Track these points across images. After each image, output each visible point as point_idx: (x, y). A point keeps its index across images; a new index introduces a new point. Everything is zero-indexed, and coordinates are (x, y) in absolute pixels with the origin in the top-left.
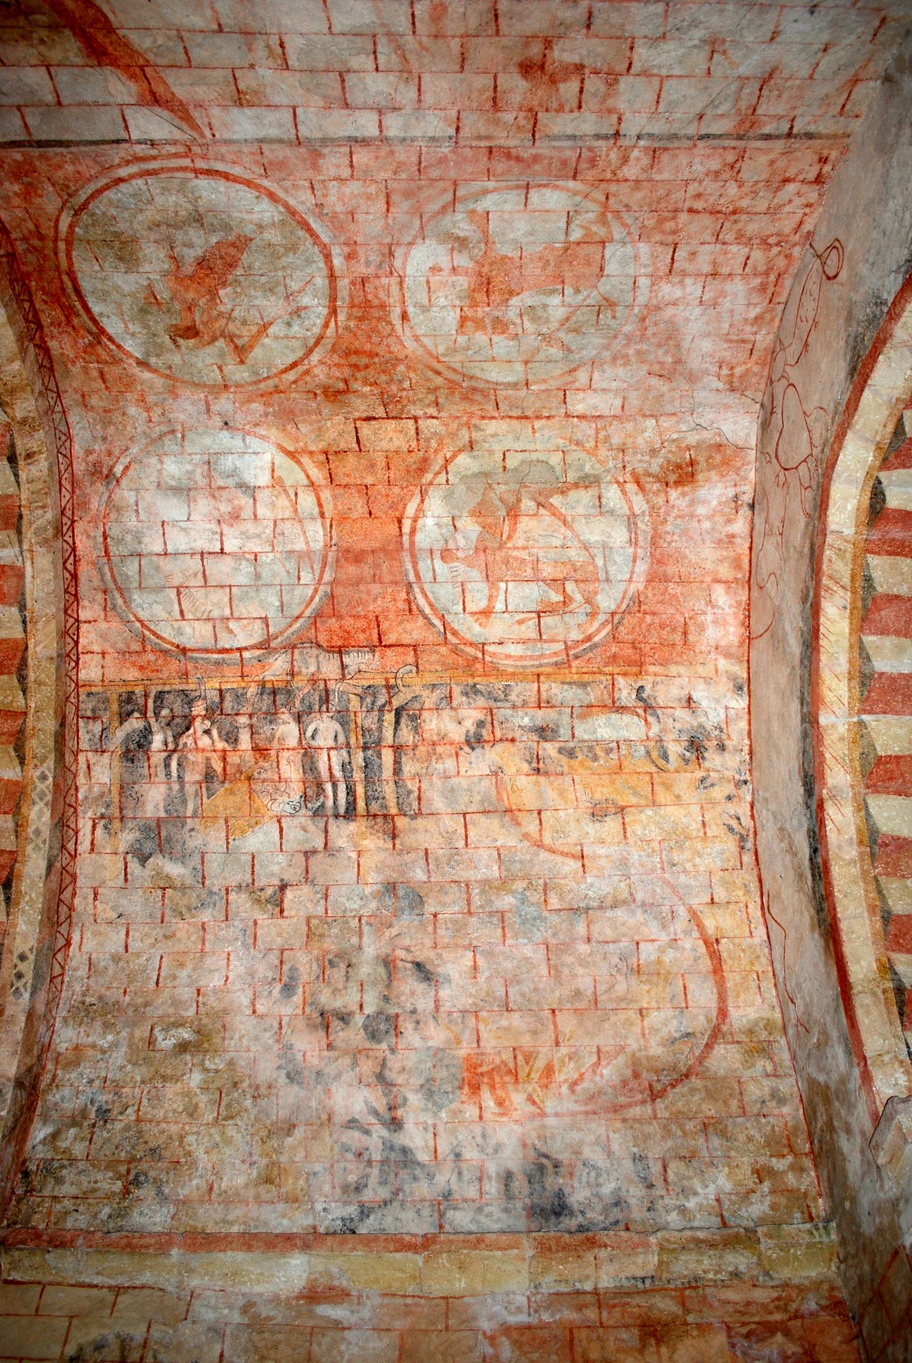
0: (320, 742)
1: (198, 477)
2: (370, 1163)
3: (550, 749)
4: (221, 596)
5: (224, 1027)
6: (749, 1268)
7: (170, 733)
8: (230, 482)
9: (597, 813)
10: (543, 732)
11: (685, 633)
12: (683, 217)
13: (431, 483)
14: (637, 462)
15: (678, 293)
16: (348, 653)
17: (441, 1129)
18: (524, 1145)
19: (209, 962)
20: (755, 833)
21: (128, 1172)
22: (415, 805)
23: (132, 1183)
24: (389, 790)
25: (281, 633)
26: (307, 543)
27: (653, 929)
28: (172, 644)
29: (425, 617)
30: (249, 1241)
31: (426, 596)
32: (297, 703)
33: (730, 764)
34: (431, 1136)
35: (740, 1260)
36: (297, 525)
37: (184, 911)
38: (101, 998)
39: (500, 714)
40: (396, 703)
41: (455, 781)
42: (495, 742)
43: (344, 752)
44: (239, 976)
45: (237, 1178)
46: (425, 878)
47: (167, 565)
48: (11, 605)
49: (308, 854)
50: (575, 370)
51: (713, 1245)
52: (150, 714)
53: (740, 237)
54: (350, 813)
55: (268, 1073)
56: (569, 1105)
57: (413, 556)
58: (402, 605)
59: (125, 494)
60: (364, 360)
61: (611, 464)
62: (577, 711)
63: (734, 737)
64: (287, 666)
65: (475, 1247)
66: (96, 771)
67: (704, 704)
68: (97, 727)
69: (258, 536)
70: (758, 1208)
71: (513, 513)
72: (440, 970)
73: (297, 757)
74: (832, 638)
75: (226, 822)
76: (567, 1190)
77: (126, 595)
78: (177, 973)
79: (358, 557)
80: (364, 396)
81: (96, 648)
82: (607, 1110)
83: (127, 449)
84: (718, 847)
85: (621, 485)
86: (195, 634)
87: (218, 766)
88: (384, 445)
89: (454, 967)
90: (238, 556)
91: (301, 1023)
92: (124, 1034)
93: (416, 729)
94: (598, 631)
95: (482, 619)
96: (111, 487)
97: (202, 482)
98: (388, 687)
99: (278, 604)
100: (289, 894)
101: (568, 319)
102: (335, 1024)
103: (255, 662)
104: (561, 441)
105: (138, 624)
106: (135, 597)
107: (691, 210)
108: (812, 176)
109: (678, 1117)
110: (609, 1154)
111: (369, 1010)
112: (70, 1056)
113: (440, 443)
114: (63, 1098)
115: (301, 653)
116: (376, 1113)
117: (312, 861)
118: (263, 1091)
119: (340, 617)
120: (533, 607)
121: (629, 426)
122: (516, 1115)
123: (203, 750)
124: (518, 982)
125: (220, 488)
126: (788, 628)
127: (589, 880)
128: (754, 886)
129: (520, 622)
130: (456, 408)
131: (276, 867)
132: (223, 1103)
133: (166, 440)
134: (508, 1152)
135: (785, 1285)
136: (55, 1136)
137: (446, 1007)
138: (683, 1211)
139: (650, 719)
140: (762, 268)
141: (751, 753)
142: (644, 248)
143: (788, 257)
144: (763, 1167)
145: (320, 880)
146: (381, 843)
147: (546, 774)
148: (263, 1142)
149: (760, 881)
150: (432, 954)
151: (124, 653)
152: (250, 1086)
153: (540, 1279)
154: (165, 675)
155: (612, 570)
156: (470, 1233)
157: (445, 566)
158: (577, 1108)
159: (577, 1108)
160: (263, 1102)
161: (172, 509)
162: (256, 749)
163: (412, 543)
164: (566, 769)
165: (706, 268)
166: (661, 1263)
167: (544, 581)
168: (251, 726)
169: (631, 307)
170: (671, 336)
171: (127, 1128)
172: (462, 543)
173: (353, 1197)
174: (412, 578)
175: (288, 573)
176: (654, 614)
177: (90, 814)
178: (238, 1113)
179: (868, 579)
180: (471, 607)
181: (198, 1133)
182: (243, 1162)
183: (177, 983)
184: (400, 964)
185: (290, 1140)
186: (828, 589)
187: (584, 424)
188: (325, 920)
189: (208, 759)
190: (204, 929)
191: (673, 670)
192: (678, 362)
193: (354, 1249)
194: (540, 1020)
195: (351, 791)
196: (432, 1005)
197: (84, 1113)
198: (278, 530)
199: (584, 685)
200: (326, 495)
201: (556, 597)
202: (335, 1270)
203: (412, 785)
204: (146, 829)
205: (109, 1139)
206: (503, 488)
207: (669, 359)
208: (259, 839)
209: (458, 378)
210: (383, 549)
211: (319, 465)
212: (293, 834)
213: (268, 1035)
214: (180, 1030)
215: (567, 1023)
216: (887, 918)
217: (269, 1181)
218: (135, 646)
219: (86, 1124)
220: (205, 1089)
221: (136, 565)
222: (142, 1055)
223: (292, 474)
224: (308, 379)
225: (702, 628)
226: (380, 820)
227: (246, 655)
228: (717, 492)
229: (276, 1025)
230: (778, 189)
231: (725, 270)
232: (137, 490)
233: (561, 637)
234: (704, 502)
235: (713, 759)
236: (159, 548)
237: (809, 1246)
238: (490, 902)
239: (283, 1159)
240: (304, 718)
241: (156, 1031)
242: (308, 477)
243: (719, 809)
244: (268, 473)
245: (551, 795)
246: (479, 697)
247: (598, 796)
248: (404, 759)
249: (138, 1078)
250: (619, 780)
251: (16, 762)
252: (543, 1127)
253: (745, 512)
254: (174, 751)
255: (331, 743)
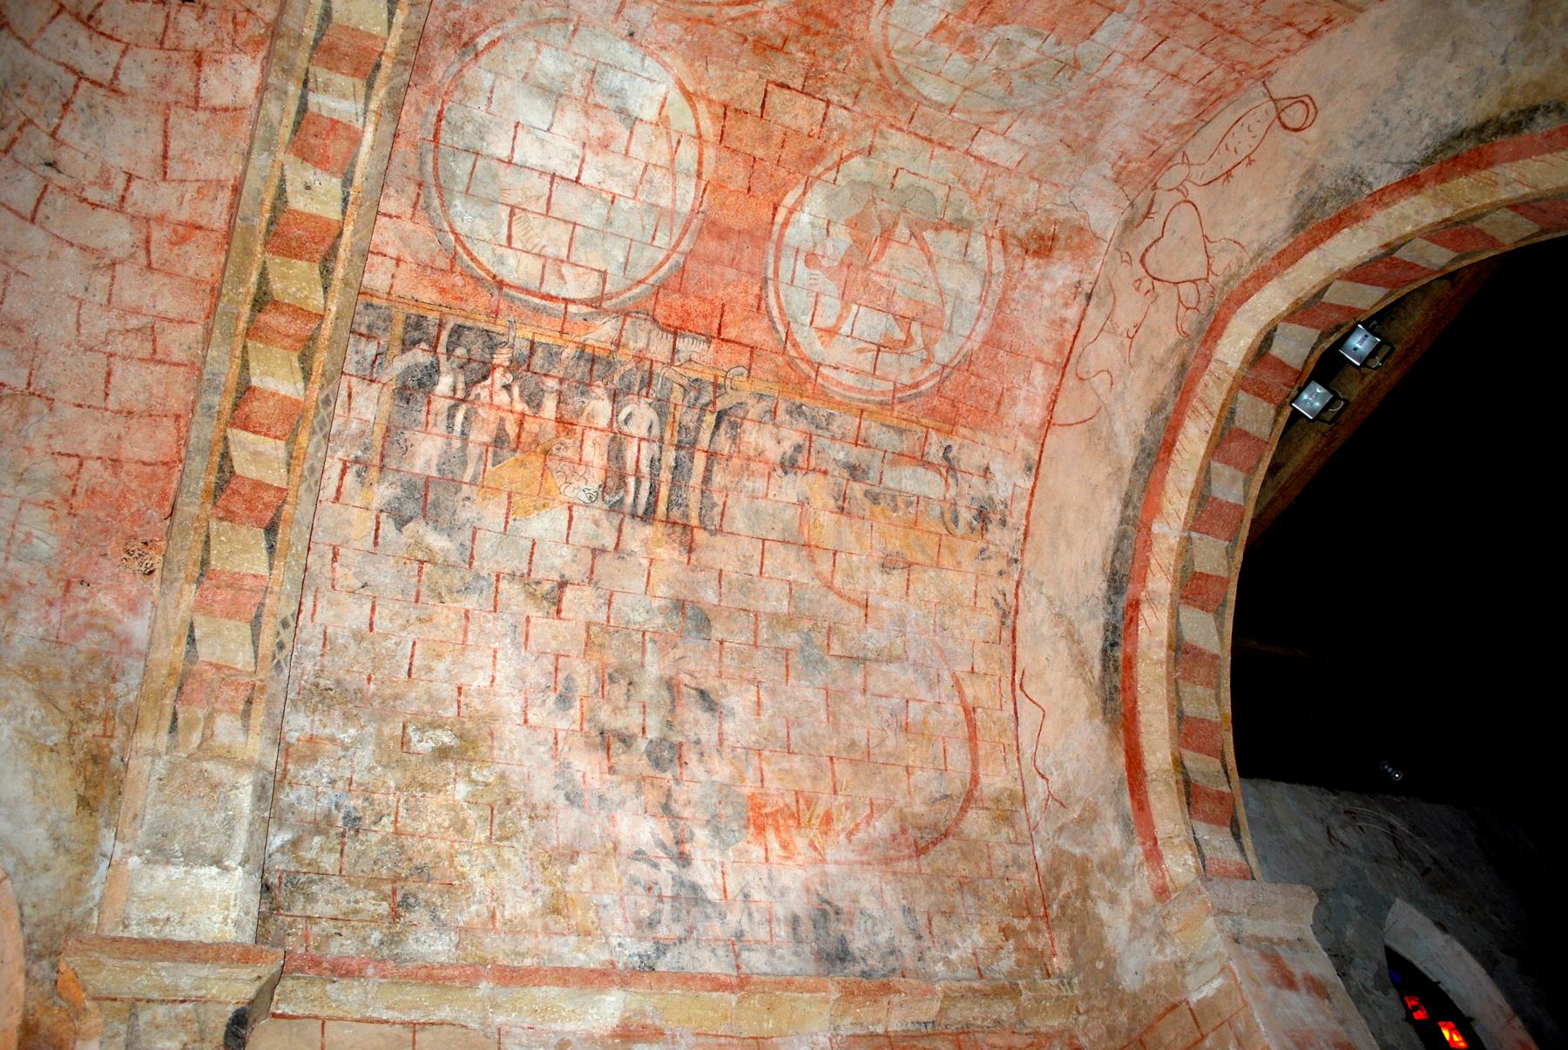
0: (632, 429)
1: (576, 84)
2: (660, 898)
3: (857, 489)
4: (563, 233)
5: (492, 734)
6: (1009, 1017)
7: (461, 378)
8: (612, 103)
9: (886, 566)
10: (855, 472)
11: (999, 403)
12: (1193, 18)
13: (818, 177)
14: (1010, 220)
15: (1136, 80)
16: (684, 337)
17: (728, 867)
18: (808, 890)
19: (471, 656)
20: (1017, 612)
21: (394, 892)
22: (717, 518)
23: (401, 906)
24: (694, 498)
25: (618, 294)
26: (674, 201)
27: (921, 691)
28: (488, 272)
29: (771, 320)
30: (564, 976)
31: (778, 297)
32: (617, 378)
33: (1007, 541)
34: (718, 875)
35: (1004, 1010)
36: (668, 177)
37: (444, 591)
38: (338, 682)
39: (819, 442)
40: (720, 405)
41: (762, 503)
42: (808, 471)
43: (655, 447)
44: (507, 678)
45: (520, 906)
46: (715, 601)
47: (507, 176)
48: (333, 174)
49: (596, 552)
50: (1002, 113)
51: (986, 995)
52: (441, 349)
53: (1219, 56)
54: (648, 516)
55: (545, 792)
56: (846, 854)
57: (778, 249)
58: (752, 301)
59: (480, 75)
60: (820, 26)
61: (986, 215)
62: (889, 456)
63: (1015, 515)
64: (614, 334)
65: (786, 989)
66: (358, 401)
67: (998, 477)
68: (371, 350)
69: (623, 176)
70: (1006, 963)
71: (887, 235)
72: (723, 701)
73: (605, 440)
74: (1186, 456)
75: (509, 497)
76: (849, 937)
77: (446, 197)
78: (433, 664)
79: (723, 234)
80: (793, 61)
81: (391, 251)
82: (880, 862)
83: (502, 20)
84: (984, 618)
85: (989, 238)
86: (518, 268)
87: (512, 430)
88: (787, 119)
89: (738, 701)
90: (595, 192)
91: (578, 740)
92: (370, 729)
93: (734, 439)
94: (927, 380)
95: (826, 338)
96: (467, 59)
97: (578, 91)
98: (716, 386)
99: (622, 260)
100: (569, 593)
101: (1031, 64)
102: (616, 746)
103: (579, 319)
104: (951, 176)
105: (452, 237)
106: (457, 202)
107: (1202, 16)
108: (1308, 29)
109: (938, 874)
110: (883, 904)
111: (652, 734)
112: (304, 748)
113: (842, 138)
114: (299, 799)
115: (633, 323)
116: (663, 846)
117: (599, 561)
118: (540, 811)
119: (685, 295)
120: (877, 339)
121: (1015, 182)
122: (800, 859)
123: (499, 408)
124: (800, 725)
125: (597, 106)
126: (1119, 427)
127: (870, 630)
128: (1008, 662)
129: (860, 351)
130: (871, 105)
131: (557, 560)
132: (496, 821)
133: (554, 27)
134: (792, 896)
135: (1036, 1033)
136: (295, 844)
137: (731, 741)
138: (947, 962)
139: (950, 480)
140: (1213, 86)
141: (1026, 534)
142: (1140, 29)
143: (1239, 85)
144: (1008, 926)
145: (605, 584)
146: (676, 555)
147: (849, 514)
148: (545, 869)
149: (1014, 658)
150: (717, 684)
151: (426, 266)
152: (526, 805)
153: (839, 1021)
154: (470, 306)
155: (957, 322)
156: (766, 974)
157: (807, 270)
158: (852, 857)
159: (852, 857)
160: (541, 824)
161: (534, 112)
162: (559, 420)
163: (781, 236)
164: (867, 514)
165: (1172, 68)
166: (941, 1009)
167: (894, 315)
168: (560, 393)
169: (1089, 75)
170: (1100, 117)
171: (384, 841)
172: (830, 251)
173: (647, 933)
174: (770, 273)
175: (644, 228)
176: (978, 376)
177: (340, 454)
178: (514, 834)
179: (1232, 412)
180: (819, 322)
181: (469, 853)
182: (525, 888)
183: (433, 677)
184: (684, 689)
185: (573, 869)
186: (1195, 410)
187: (978, 167)
188: (606, 628)
189: (502, 420)
190: (467, 617)
191: (981, 436)
192: (1092, 139)
193: (671, 987)
194: (818, 765)
195: (654, 491)
196: (715, 738)
197: (328, 817)
198: (646, 177)
199: (901, 432)
200: (710, 153)
201: (900, 335)
202: (648, 1008)
203: (718, 498)
204: (409, 487)
205: (364, 853)
206: (885, 206)
207: (1086, 135)
208: (544, 525)
209: (893, 78)
210: (750, 233)
211: (714, 118)
212: (583, 527)
213: (542, 749)
214: (439, 732)
215: (843, 771)
216: (1181, 718)
217: (556, 911)
218: (442, 263)
219: (333, 832)
220: (473, 802)
221: (469, 164)
222: (395, 757)
223: (682, 118)
224: (750, 21)
225: (1014, 402)
226: (679, 529)
227: (572, 308)
228: (1065, 273)
229: (551, 740)
230: (1279, 28)
231: (1184, 76)
232: (497, 74)
233: (892, 377)
234: (1053, 280)
235: (995, 533)
236: (504, 153)
237: (1058, 998)
238: (776, 637)
239: (569, 888)
240: (620, 398)
241: (410, 729)
242: (698, 126)
243: (991, 582)
244: (656, 106)
245: (849, 538)
246: (802, 419)
247: (890, 548)
248: (715, 468)
249: (392, 784)
250: (913, 534)
251: (299, 376)
252: (825, 873)
253: (1081, 299)
254: (463, 400)
255: (644, 433)
